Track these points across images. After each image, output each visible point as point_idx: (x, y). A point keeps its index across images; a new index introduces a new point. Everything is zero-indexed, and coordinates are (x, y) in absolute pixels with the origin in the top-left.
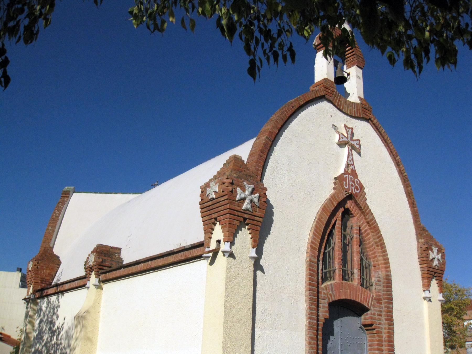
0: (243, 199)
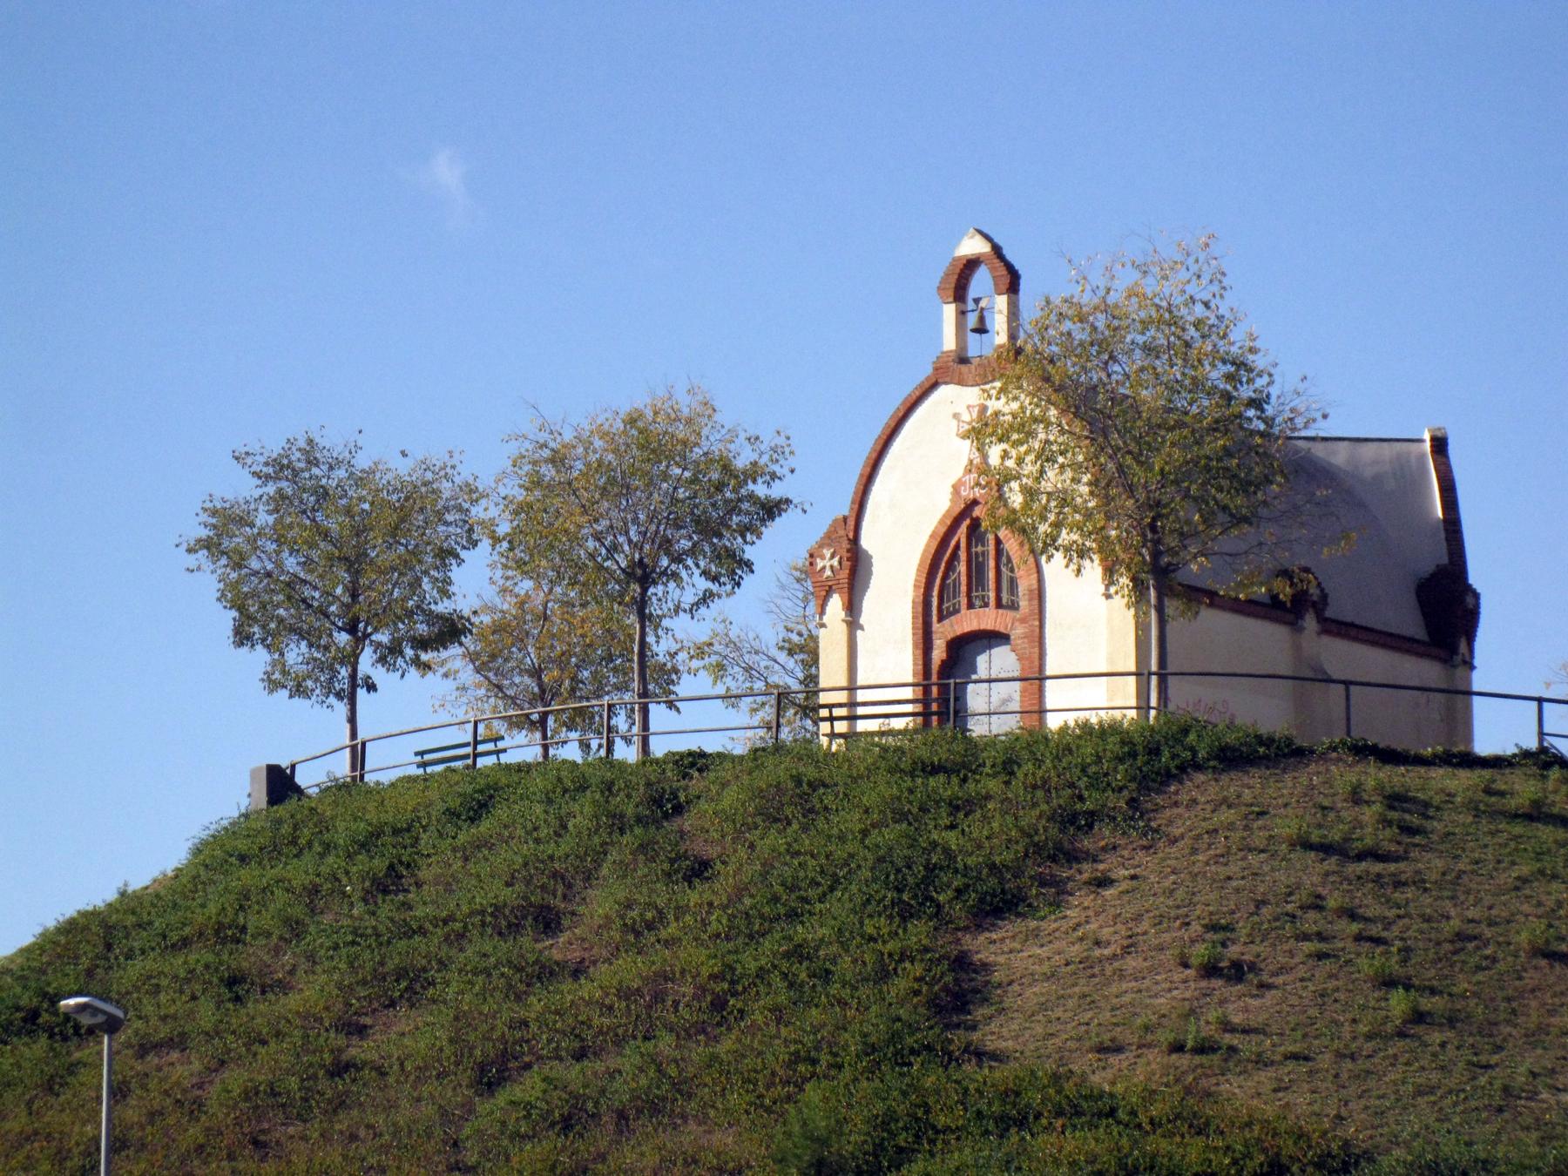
0: (824, 568)
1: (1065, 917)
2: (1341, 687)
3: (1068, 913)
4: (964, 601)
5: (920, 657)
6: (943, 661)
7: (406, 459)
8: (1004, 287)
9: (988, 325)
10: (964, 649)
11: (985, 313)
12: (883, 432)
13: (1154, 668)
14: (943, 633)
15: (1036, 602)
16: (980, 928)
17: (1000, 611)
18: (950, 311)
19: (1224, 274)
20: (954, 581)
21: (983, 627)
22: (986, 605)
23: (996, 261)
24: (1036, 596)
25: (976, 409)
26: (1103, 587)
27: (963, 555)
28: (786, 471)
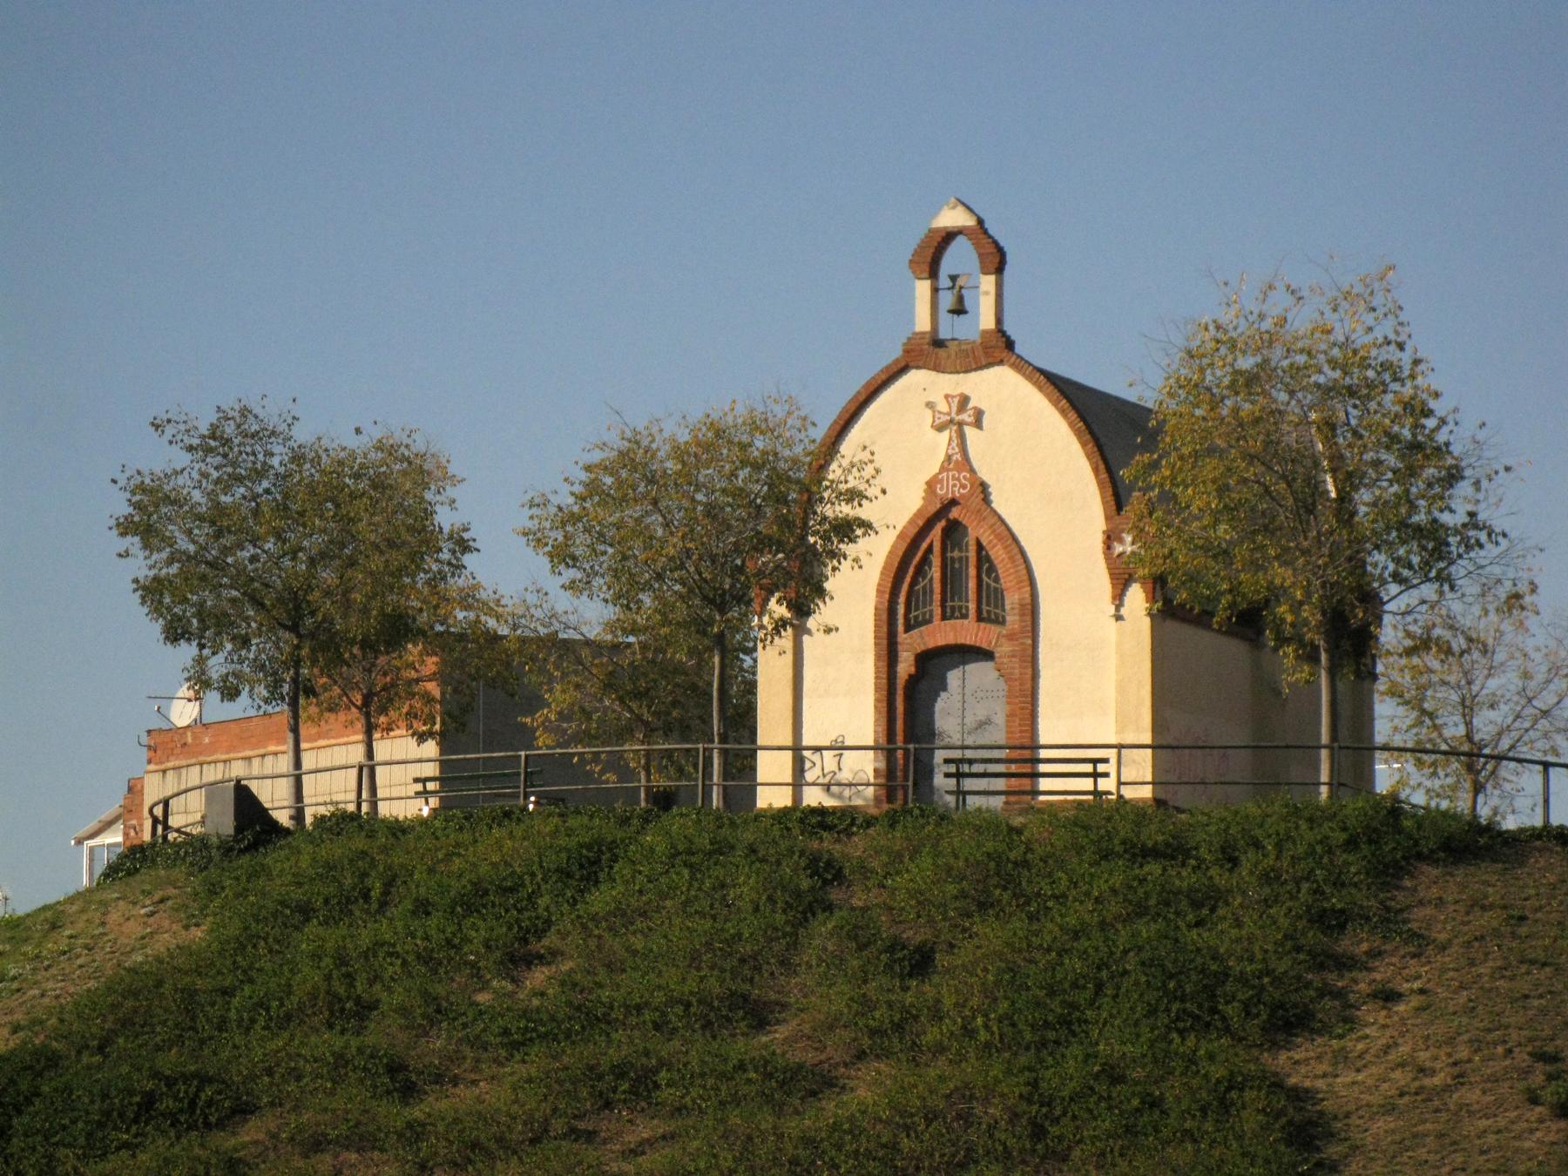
1: (1367, 1037)
2: (1540, 768)
3: (1367, 1031)
4: (937, 611)
5: (885, 670)
6: (910, 676)
7: (360, 437)
8: (993, 267)
9: (968, 304)
10: (935, 664)
11: (963, 291)
12: (839, 417)
13: (1325, 738)
14: (911, 645)
15: (1028, 618)
16: (1275, 1046)
17: (983, 625)
18: (923, 288)
19: (1401, 308)
20: (924, 587)
21: (961, 641)
22: (965, 616)
23: (982, 236)
24: (1029, 612)
25: (956, 400)
26: (1113, 608)
27: (936, 560)
28: (877, 491)
